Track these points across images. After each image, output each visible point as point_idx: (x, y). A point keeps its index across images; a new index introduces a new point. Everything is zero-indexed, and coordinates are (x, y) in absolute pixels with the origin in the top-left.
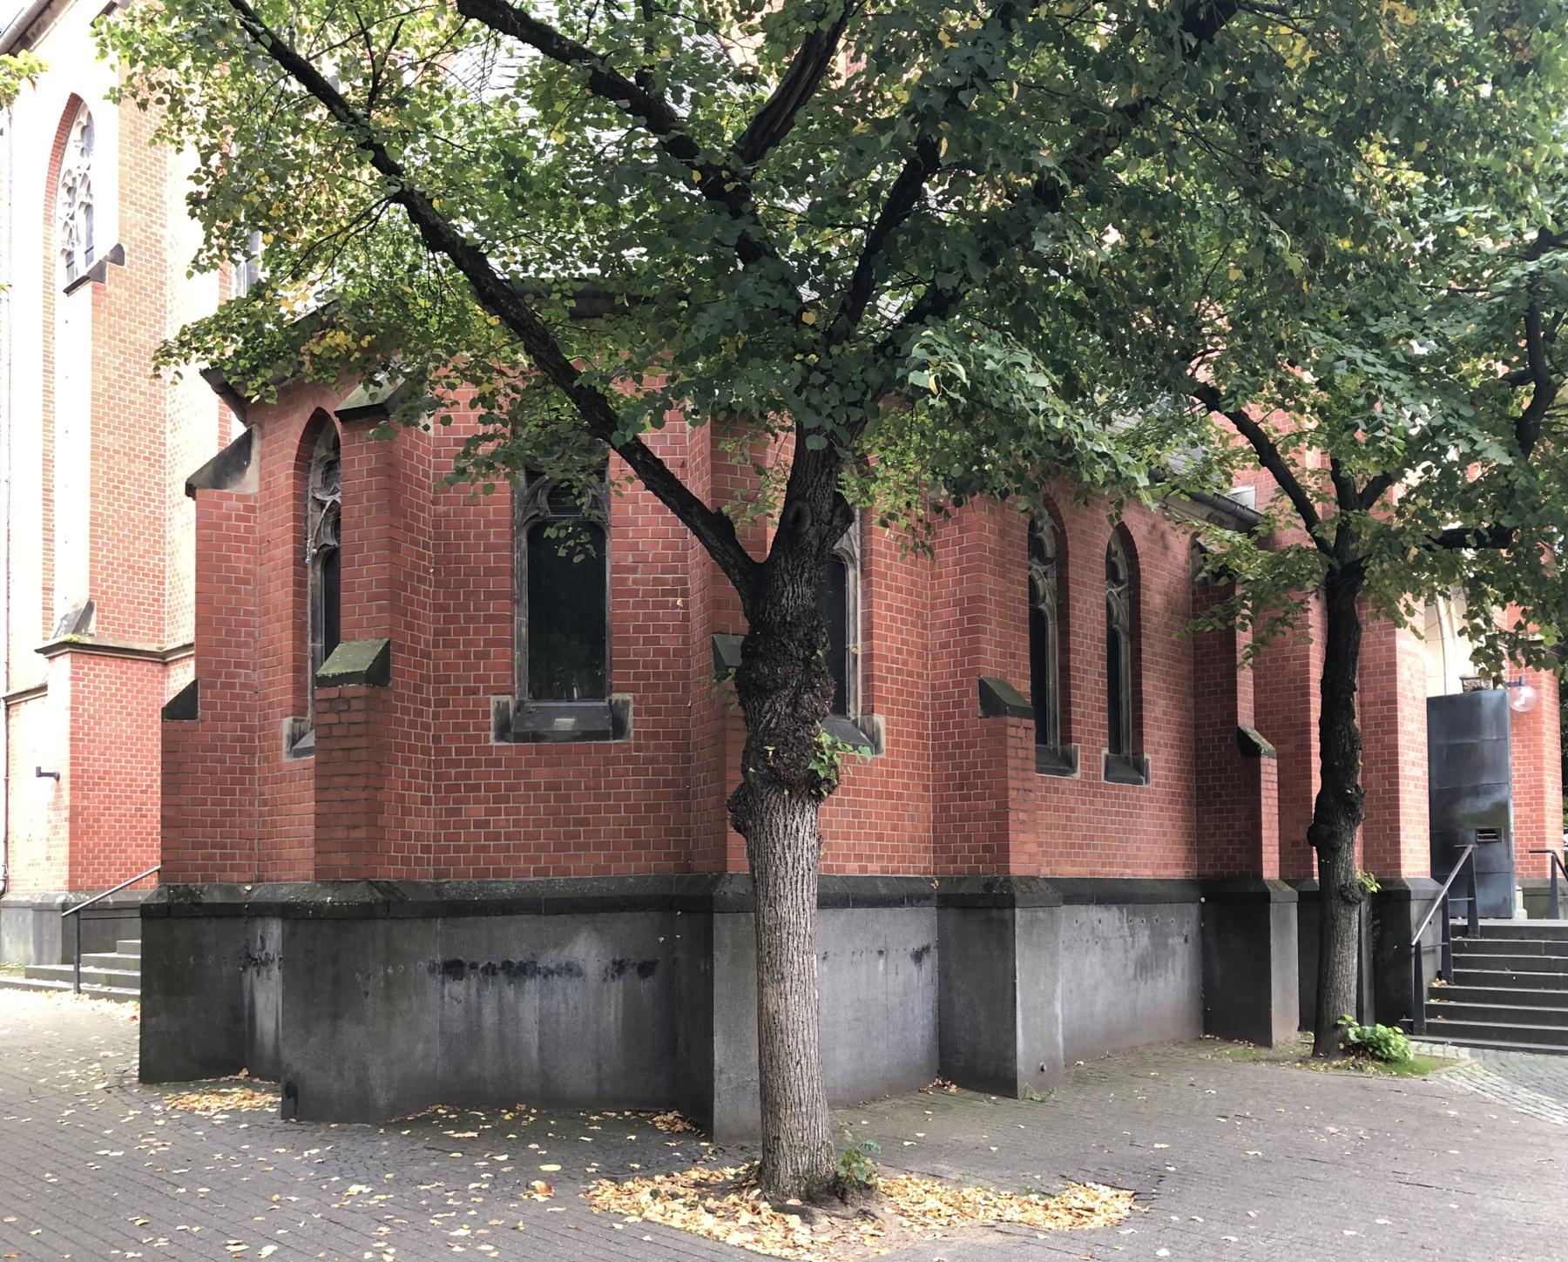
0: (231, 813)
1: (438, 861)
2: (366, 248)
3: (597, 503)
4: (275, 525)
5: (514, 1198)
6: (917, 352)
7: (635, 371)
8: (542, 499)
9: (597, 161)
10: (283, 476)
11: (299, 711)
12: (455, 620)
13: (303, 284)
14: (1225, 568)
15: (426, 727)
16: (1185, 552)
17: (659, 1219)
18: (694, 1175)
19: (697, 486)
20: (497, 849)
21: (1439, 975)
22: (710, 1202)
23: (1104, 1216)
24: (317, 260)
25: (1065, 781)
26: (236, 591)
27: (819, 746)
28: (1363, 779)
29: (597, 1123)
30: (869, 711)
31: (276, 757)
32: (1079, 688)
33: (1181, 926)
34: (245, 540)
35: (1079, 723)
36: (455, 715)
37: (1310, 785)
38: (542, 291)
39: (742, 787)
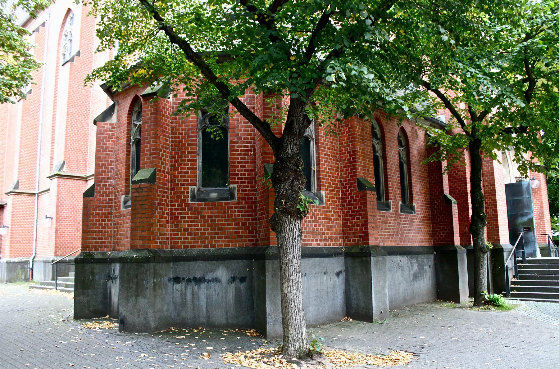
0: (104, 228)
1: (171, 243)
2: (152, 44)
3: (225, 121)
4: (121, 133)
5: (196, 358)
6: (329, 70)
7: (237, 77)
8: (207, 121)
9: (225, 15)
10: (124, 117)
11: (127, 193)
12: (177, 161)
13: (131, 55)
14: (436, 141)
15: (167, 197)
16: (423, 136)
17: (247, 366)
18: (260, 350)
19: (258, 114)
20: (192, 238)
21: (514, 277)
22: (265, 360)
23: (403, 361)
24: (136, 48)
25: (387, 213)
26: (108, 154)
27: (301, 200)
28: (486, 211)
29: (226, 333)
30: (319, 190)
31: (119, 209)
32: (390, 181)
33: (428, 262)
34: (112, 138)
35: (391, 193)
36: (177, 193)
37: (468, 213)
38: (208, 55)
39: (274, 215)
